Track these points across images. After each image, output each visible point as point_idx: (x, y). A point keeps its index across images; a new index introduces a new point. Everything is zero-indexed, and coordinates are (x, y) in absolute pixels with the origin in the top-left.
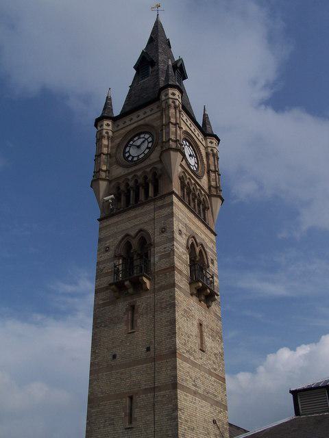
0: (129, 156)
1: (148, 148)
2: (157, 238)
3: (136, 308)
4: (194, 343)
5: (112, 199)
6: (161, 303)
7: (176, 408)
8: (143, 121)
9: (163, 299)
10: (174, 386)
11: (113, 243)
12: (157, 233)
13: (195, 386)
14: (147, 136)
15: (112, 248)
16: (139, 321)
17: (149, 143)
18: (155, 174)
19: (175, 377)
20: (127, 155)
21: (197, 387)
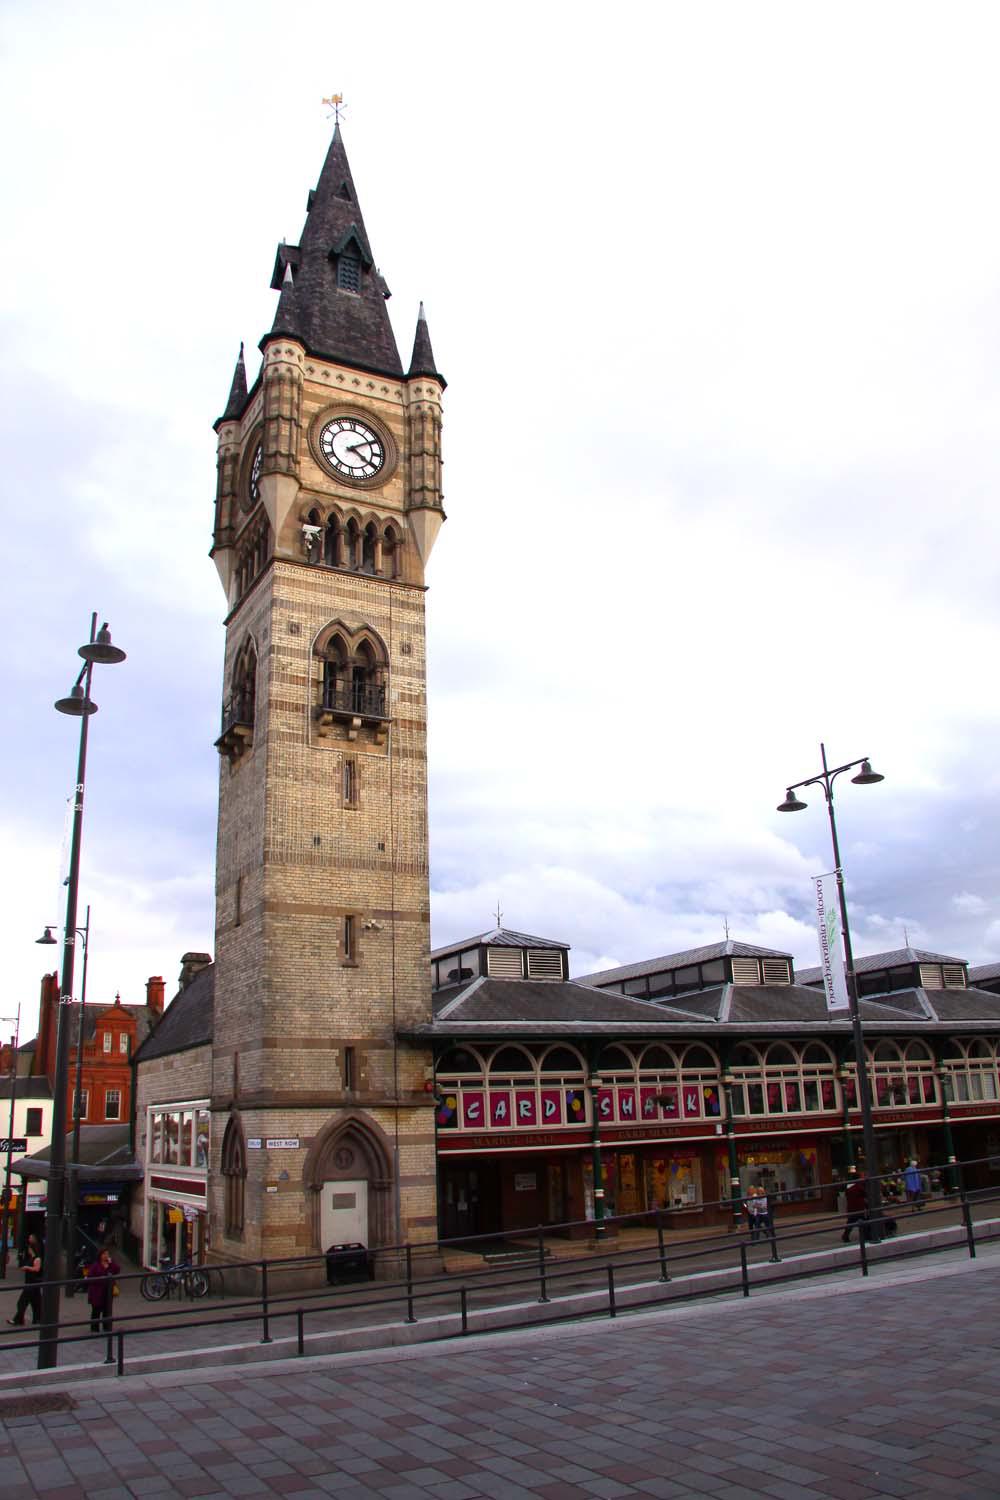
16: (363, 793)
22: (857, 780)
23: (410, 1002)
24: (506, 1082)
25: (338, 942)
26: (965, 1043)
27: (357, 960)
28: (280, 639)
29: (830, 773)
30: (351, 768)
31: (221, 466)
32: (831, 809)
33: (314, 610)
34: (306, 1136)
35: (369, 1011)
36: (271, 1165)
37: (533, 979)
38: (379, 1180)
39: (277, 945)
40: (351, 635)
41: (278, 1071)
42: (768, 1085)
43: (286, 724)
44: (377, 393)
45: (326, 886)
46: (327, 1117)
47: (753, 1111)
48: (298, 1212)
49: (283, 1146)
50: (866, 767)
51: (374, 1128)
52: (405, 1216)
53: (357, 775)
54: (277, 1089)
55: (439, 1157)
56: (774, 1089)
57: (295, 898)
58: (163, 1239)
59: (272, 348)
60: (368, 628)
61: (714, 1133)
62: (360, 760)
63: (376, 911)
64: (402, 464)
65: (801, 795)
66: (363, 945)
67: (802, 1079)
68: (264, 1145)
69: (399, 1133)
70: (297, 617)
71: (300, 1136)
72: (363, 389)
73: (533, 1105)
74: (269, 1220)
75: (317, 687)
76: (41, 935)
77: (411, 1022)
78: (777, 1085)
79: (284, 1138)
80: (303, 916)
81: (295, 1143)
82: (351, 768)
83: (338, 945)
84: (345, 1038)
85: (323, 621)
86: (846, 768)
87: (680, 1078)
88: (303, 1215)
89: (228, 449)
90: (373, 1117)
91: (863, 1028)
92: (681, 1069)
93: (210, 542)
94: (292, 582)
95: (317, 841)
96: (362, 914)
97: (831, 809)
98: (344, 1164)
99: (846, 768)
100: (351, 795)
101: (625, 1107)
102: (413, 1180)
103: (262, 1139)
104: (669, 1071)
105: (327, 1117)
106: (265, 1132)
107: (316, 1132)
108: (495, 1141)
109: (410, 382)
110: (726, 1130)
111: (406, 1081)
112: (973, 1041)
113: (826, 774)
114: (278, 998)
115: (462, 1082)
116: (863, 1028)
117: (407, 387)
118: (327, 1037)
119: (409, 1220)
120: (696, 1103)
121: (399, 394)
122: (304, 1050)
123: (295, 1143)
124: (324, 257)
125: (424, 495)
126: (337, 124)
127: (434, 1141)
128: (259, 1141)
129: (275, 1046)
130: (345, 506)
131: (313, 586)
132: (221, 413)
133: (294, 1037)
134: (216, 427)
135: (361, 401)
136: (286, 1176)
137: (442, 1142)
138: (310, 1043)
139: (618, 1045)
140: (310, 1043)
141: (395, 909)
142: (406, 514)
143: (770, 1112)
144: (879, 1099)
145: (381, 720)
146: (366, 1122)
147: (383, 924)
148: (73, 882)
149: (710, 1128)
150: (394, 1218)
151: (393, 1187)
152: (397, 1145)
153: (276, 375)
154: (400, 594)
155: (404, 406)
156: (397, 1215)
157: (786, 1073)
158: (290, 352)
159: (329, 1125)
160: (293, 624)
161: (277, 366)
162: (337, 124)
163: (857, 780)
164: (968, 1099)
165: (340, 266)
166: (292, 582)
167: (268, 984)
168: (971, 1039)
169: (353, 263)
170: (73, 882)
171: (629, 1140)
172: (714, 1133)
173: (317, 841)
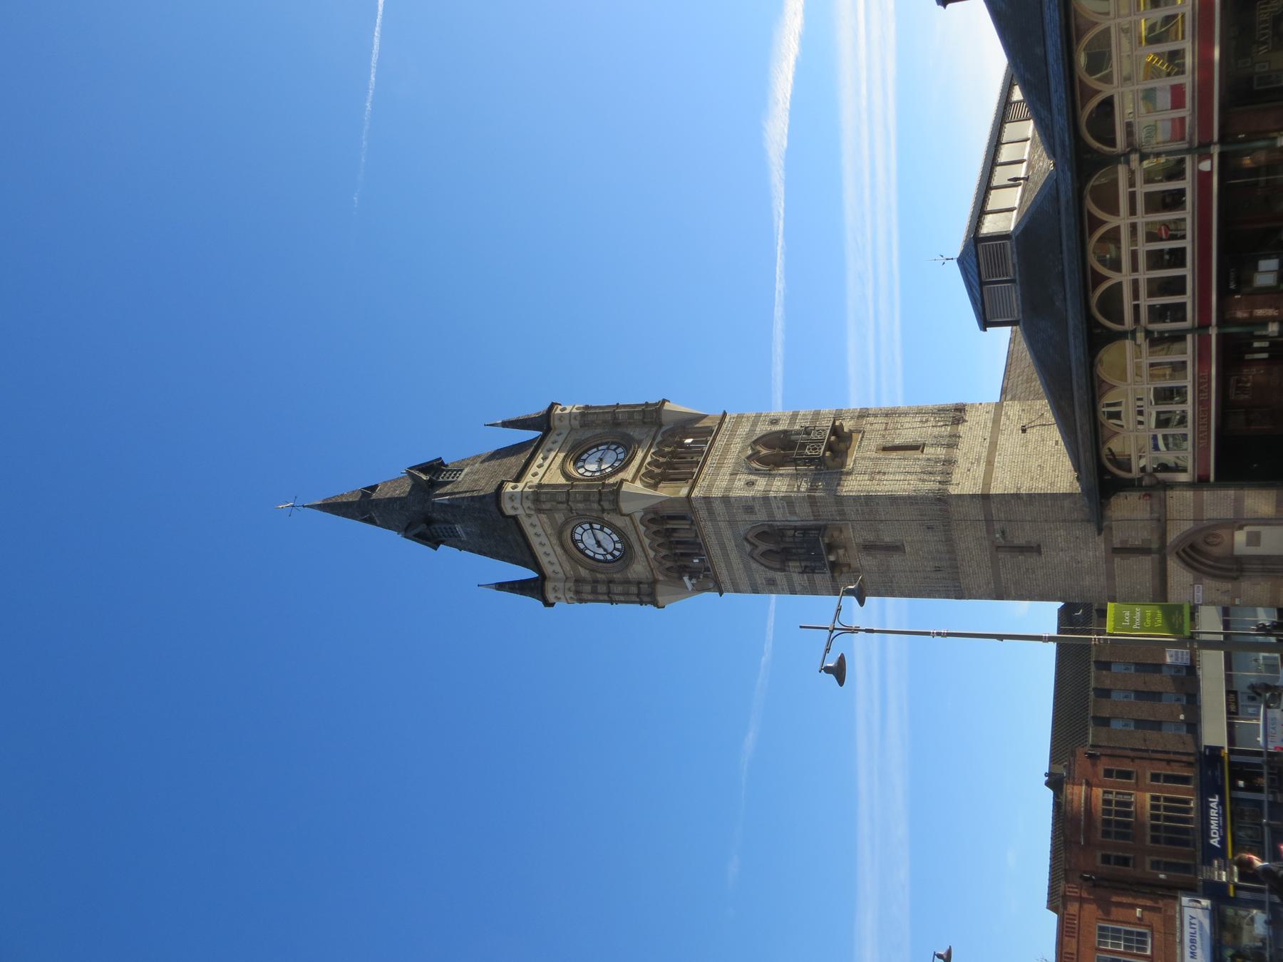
0: (618, 550)
1: (601, 530)
2: (761, 516)
3: (867, 543)
4: (913, 461)
5: (690, 579)
6: (863, 514)
7: (1017, 496)
8: (552, 539)
9: (857, 510)
10: (985, 498)
11: (761, 574)
12: (754, 518)
13: (978, 460)
14: (579, 530)
15: (771, 574)
16: (887, 539)
17: (603, 510)
18: (652, 521)
19: (973, 496)
20: (609, 557)
21: (980, 457)
24: (1132, 196)
25: (1020, 557)
27: (1034, 545)
31: (581, 601)
34: (1192, 580)
35: (1077, 538)
37: (1015, 274)
46: (1174, 566)
47: (1182, 291)
48: (1259, 586)
53: (874, 544)
54: (1151, 596)
56: (1156, 260)
61: (1210, 174)
62: (860, 540)
63: (988, 531)
66: (1020, 540)
67: (1144, 275)
69: (1192, 518)
71: (1192, 583)
72: (548, 549)
77: (1084, 509)
78: (1148, 196)
79: (1194, 593)
80: (1003, 579)
83: (1023, 557)
84: (1104, 554)
87: (1135, 276)
88: (1262, 583)
90: (1175, 536)
96: (993, 542)
100: (896, 548)
105: (1174, 566)
107: (1188, 574)
114: (1074, 594)
115: (1134, 300)
118: (1104, 565)
122: (1117, 579)
132: (540, 603)
138: (1110, 576)
140: (1110, 576)
141: (983, 519)
143: (1184, 209)
144: (1173, 238)
145: (824, 543)
147: (997, 526)
148: (1001, 637)
149: (1204, 178)
152: (1203, 520)
157: (1136, 296)
159: (1183, 566)
160: (770, 580)
164: (1184, 363)
170: (1001, 637)
171: (1210, 395)
172: (1210, 174)
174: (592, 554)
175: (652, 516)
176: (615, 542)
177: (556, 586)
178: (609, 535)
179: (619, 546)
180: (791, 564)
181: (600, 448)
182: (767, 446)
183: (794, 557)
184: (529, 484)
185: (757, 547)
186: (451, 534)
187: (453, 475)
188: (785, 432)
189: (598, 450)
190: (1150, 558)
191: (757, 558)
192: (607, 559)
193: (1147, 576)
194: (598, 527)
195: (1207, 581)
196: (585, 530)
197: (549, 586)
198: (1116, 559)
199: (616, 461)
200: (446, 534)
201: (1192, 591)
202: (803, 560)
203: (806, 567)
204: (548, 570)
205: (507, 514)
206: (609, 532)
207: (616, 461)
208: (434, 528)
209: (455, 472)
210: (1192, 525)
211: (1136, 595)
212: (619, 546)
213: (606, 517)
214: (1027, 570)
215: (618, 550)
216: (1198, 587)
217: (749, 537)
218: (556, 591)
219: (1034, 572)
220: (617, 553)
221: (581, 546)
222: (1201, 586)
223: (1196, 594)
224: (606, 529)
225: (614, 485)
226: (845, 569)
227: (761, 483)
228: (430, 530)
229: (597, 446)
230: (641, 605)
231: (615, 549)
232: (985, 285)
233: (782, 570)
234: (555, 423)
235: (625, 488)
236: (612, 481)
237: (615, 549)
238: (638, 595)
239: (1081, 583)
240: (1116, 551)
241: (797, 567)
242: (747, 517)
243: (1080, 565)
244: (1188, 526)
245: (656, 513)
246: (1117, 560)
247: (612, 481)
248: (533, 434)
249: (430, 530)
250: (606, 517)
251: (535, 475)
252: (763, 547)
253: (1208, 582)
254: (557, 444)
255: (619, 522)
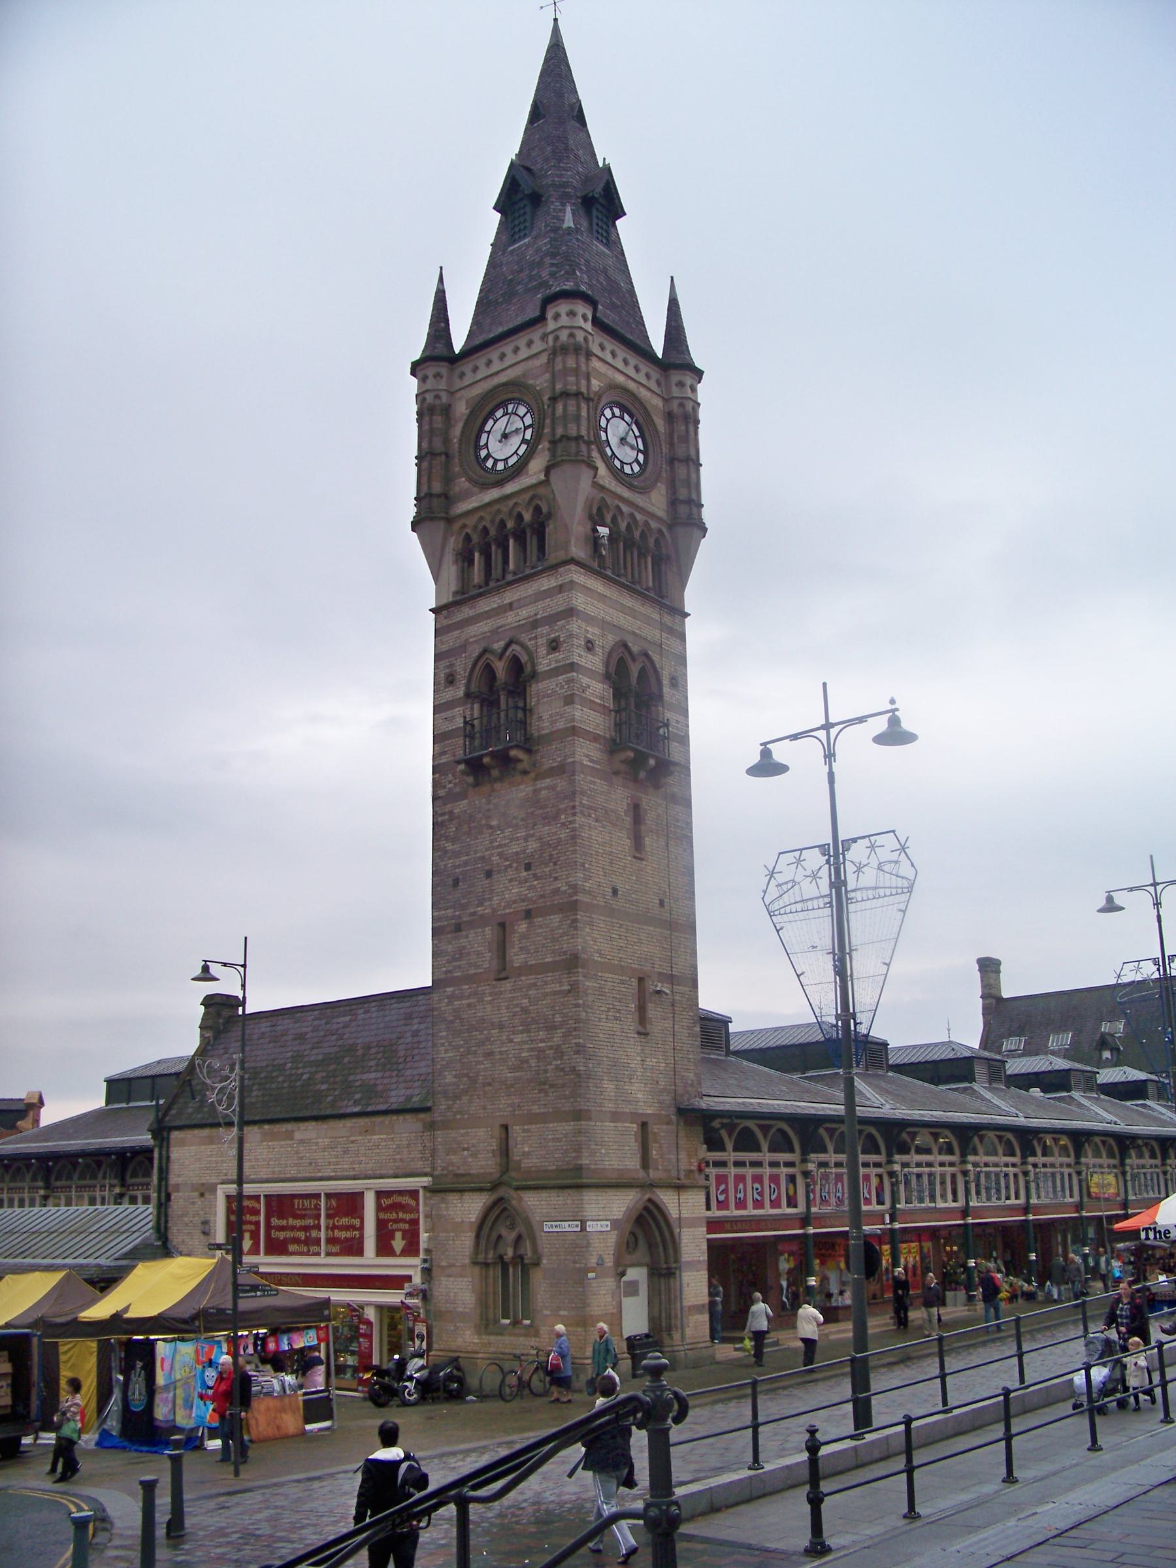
0: (495, 464)
1: (524, 441)
11: (462, 666)
14: (522, 410)
20: (483, 453)
22: (880, 739)
23: (686, 1074)
26: (730, 1128)
28: (580, 656)
29: (833, 725)
30: (636, 813)
32: (1159, 917)
33: (605, 625)
36: (591, 1249)
38: (665, 1266)
39: (589, 1007)
40: (634, 660)
41: (594, 1147)
42: (735, 1176)
43: (588, 756)
44: (641, 378)
45: (622, 943)
48: (611, 1299)
49: (567, 1223)
50: (894, 721)
51: (662, 1207)
52: (686, 1303)
55: (709, 1240)
57: (601, 955)
58: (125, 1340)
59: (420, 374)
60: (646, 655)
63: (660, 974)
64: (664, 466)
65: (780, 753)
68: (583, 1229)
70: (593, 632)
73: (762, 1186)
74: (590, 1309)
75: (609, 716)
76: (198, 971)
79: (598, 1220)
80: (607, 975)
81: (577, 1226)
82: (636, 813)
85: (612, 639)
86: (861, 720)
89: (437, 397)
91: (858, 1114)
92: (833, 1155)
93: (412, 511)
94: (587, 590)
95: (615, 892)
97: (1159, 917)
98: (631, 1250)
99: (861, 720)
101: (738, 1196)
102: (692, 1265)
103: (581, 1221)
104: (754, 1156)
106: (585, 1214)
107: (622, 1213)
108: (728, 1226)
109: (672, 372)
110: (892, 1220)
111: (686, 1162)
112: (839, 1131)
113: (827, 726)
116: (858, 1114)
117: (667, 377)
119: (689, 1307)
120: (870, 1193)
121: (658, 383)
122: (612, 1124)
123: (577, 1226)
124: (577, 197)
125: (691, 509)
126: (556, 20)
127: (705, 1225)
128: (579, 1223)
129: (590, 1119)
130: (625, 509)
131: (602, 598)
132: (417, 356)
133: (604, 1109)
134: (415, 368)
135: (631, 386)
136: (601, 1260)
137: (713, 1225)
139: (751, 1124)
140: (616, 1117)
142: (671, 527)
146: (658, 1202)
150: (678, 1305)
151: (678, 1272)
153: (572, 341)
154: (667, 619)
155: (663, 398)
156: (681, 1304)
158: (572, 314)
161: (558, 333)
162: (556, 20)
163: (880, 739)
165: (595, 213)
166: (587, 590)
167: (580, 1050)
168: (774, 1125)
169: (605, 212)
171: (737, 1232)
173: (615, 892)
174: (487, 428)
175: (545, 510)
176: (506, 460)
177: (442, 377)
178: (516, 452)
179: (500, 466)
180: (476, 706)
181: (639, 440)
182: (643, 671)
183: (485, 713)
184: (590, 337)
185: (500, 659)
186: (517, 229)
187: (600, 231)
188: (660, 697)
189: (636, 437)
190: (638, 1167)
191: (483, 660)
192: (480, 449)
193: (616, 1163)
194: (528, 436)
195: (615, 1236)
196: (522, 418)
197: (443, 368)
198: (635, 1125)
199: (621, 462)
200: (517, 222)
201: (601, 1218)
202: (481, 723)
203: (473, 726)
204: (466, 367)
205: (549, 307)
206: (521, 452)
207: (621, 462)
208: (525, 206)
209: (604, 234)
210: (674, 1216)
211: (594, 1147)
212: (500, 466)
213: (544, 445)
214: (619, 1011)
215: (495, 464)
216: (607, 1226)
217: (514, 646)
218: (435, 377)
219: (616, 1018)
220: (490, 464)
221: (499, 413)
222: (609, 1229)
223: (599, 1223)
224: (524, 447)
225: (590, 457)
226: (470, 779)
227: (595, 662)
228: (521, 200)
229: (642, 436)
230: (415, 499)
231: (496, 461)
232: (249, 1020)
233: (468, 695)
234: (675, 377)
235: (586, 476)
236: (595, 454)
237: (496, 461)
238: (430, 495)
239: (606, 1078)
240: (644, 1125)
241: (472, 715)
242: (542, 641)
243: (627, 1080)
244: (673, 1212)
245: (549, 515)
246: (634, 1127)
247: (595, 454)
248: (658, 347)
249: (521, 200)
250: (544, 445)
251: (602, 348)
252: (500, 667)
253: (613, 1238)
254: (634, 371)
255: (537, 466)
